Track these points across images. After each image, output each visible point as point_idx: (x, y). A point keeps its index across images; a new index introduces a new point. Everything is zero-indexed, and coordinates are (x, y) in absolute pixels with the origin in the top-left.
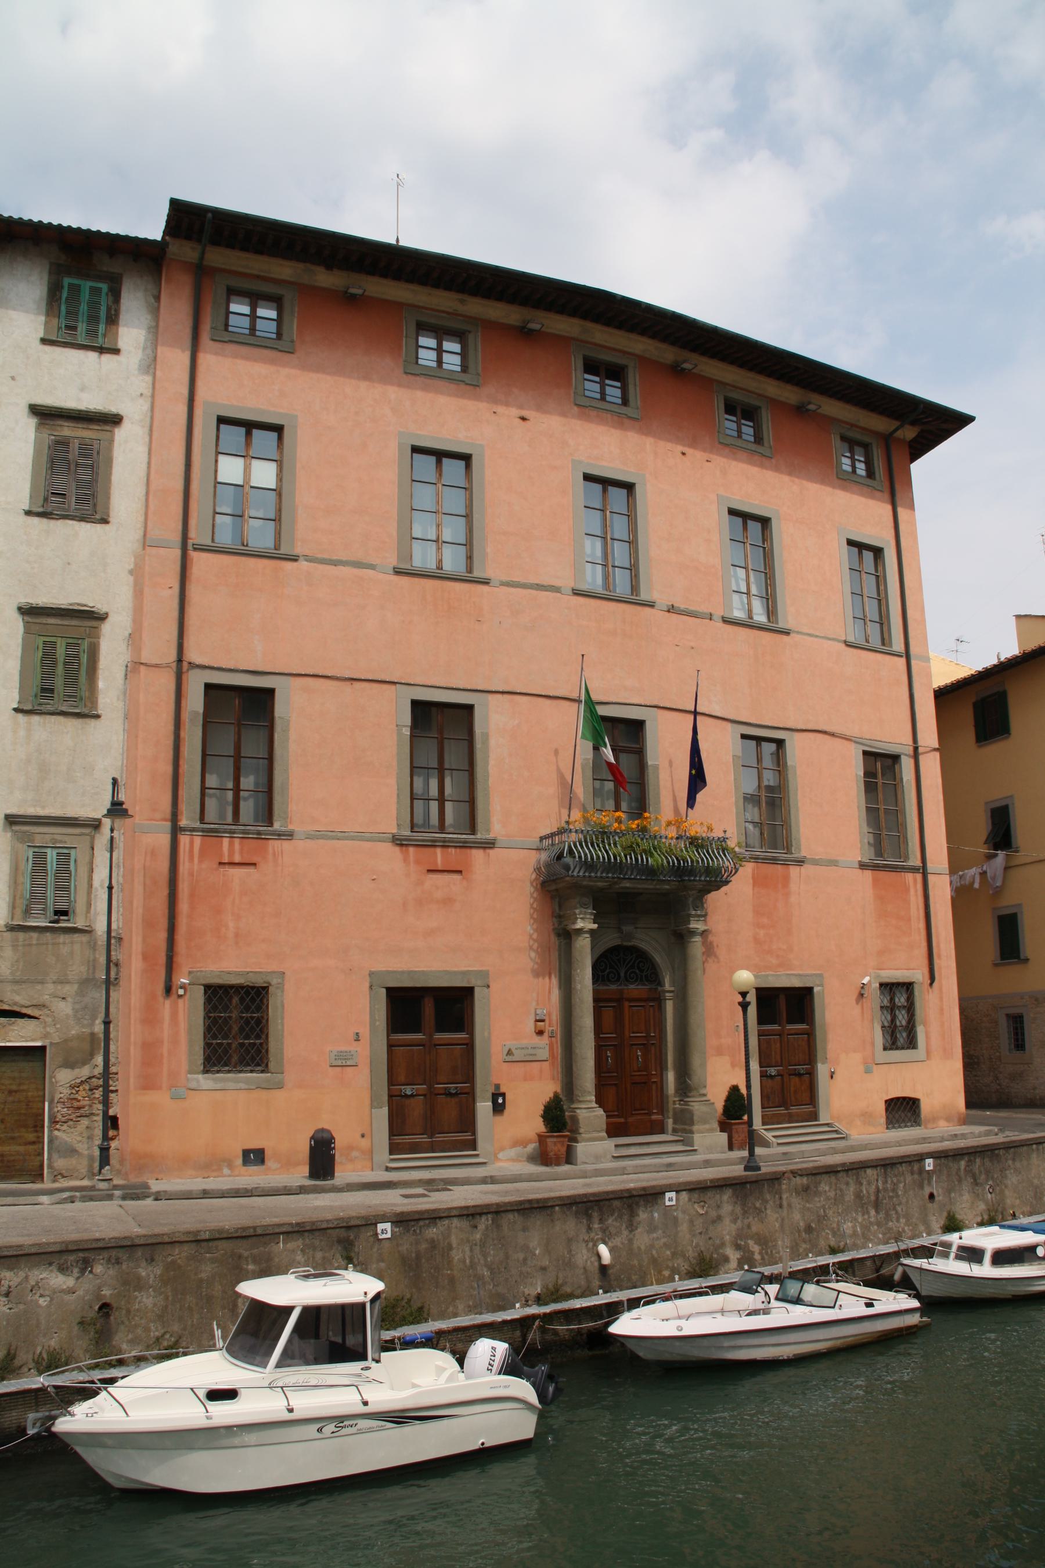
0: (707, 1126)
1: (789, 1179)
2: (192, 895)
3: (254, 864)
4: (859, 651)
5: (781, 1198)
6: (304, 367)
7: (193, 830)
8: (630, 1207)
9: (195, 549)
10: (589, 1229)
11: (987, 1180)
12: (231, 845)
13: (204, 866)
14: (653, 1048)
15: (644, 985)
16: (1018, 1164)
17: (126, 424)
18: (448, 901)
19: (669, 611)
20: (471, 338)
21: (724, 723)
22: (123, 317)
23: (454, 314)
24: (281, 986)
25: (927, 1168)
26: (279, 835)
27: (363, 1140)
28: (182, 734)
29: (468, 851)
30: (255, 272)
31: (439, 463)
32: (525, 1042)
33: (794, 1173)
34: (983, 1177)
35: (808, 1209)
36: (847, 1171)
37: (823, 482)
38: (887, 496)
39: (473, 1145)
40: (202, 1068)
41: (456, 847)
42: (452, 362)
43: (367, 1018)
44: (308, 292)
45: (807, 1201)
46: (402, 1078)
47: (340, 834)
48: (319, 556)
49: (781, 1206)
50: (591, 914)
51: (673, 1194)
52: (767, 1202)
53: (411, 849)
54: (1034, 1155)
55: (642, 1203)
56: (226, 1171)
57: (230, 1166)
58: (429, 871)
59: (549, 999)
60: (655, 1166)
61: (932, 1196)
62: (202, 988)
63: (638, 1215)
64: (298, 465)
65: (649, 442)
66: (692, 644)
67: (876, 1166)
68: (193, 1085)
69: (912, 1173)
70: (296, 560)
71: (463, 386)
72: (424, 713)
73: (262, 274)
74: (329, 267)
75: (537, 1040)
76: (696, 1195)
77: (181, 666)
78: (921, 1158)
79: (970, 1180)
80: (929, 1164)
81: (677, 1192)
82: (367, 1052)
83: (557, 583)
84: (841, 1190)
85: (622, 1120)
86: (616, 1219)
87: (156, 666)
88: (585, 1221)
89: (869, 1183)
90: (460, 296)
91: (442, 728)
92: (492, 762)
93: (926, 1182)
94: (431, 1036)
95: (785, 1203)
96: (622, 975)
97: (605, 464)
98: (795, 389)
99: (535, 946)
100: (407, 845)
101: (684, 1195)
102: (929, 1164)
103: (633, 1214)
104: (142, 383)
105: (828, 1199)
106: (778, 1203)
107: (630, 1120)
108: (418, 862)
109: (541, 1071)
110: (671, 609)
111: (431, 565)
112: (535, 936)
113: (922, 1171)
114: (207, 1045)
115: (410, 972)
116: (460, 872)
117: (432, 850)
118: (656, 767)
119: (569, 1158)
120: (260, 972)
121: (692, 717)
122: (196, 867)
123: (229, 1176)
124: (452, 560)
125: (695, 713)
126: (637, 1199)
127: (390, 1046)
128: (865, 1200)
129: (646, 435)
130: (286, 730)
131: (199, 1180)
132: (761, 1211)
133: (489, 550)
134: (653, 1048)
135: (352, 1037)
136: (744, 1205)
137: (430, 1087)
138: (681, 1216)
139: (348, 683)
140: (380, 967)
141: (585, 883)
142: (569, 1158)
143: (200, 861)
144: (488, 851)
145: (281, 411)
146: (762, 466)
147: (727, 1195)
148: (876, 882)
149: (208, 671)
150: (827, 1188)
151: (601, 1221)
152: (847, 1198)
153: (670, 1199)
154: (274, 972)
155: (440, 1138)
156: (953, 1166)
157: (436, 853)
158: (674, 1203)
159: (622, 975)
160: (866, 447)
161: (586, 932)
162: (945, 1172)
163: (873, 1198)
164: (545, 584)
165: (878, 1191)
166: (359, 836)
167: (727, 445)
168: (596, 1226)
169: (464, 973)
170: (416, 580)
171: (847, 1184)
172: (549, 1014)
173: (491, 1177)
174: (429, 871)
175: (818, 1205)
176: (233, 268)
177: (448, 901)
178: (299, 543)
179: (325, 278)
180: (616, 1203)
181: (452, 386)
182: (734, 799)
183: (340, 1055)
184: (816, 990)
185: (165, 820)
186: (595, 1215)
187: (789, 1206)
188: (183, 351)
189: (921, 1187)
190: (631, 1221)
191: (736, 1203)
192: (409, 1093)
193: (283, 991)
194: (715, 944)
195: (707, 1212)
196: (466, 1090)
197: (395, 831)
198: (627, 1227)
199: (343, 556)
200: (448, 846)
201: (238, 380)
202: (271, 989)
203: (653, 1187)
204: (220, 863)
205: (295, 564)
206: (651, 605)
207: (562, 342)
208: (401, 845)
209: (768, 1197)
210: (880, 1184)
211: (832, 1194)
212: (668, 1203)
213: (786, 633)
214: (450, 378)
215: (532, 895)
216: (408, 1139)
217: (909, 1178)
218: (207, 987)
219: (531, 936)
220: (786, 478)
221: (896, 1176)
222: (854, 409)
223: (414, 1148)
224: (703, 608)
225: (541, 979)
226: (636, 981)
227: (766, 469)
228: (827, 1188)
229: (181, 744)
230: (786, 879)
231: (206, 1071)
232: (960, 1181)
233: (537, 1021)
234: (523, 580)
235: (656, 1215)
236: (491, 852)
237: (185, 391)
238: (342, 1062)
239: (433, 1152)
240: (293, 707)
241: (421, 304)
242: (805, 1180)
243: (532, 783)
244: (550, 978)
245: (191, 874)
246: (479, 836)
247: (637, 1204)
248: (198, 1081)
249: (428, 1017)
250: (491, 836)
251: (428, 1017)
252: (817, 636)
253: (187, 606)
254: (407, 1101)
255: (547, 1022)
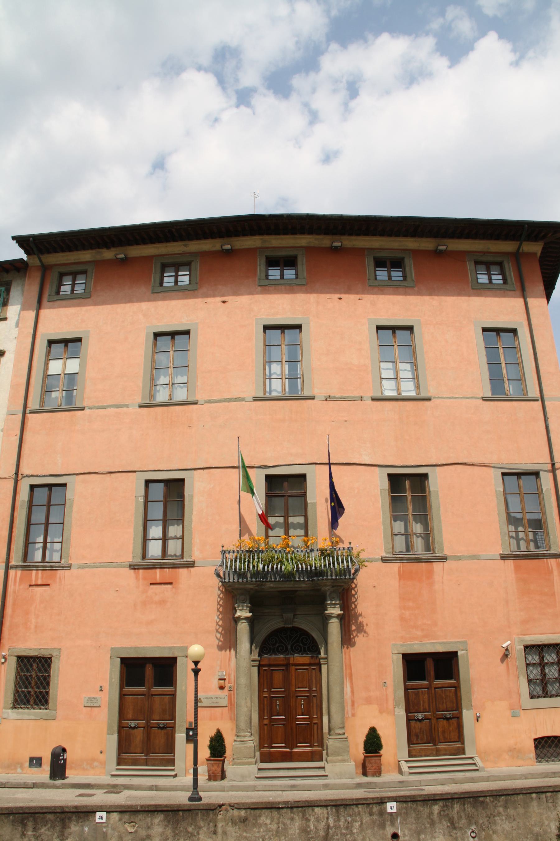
0: (340, 758)
1: (227, 810)
2: (14, 604)
3: (49, 585)
4: (496, 402)
5: (215, 826)
6: (95, 304)
7: (16, 567)
8: (63, 821)
9: (30, 413)
10: (23, 835)
11: (470, 824)
12: (37, 574)
13: (21, 587)
14: (315, 699)
15: (307, 654)
16: (511, 811)
17: (7, 355)
18: (162, 602)
19: (326, 400)
20: (193, 264)
21: (373, 468)
22: (11, 301)
23: (184, 254)
24: (59, 656)
25: (389, 811)
26: (63, 567)
27: (101, 755)
28: (15, 514)
29: (177, 570)
30: (73, 261)
31: (394, 333)
32: (211, 694)
33: (232, 806)
34: (464, 821)
35: (246, 837)
36: (292, 808)
37: (459, 294)
38: (519, 292)
39: (172, 762)
40: (12, 705)
41: (169, 568)
42: (184, 279)
43: (108, 676)
44: (99, 264)
45: (245, 831)
46: (130, 716)
47: (93, 564)
48: (96, 405)
49: (215, 833)
50: (247, 607)
51: (104, 814)
52: (200, 828)
53: (141, 571)
54: (535, 803)
55: (74, 818)
56: (19, 770)
57: (22, 767)
58: (151, 584)
59: (229, 665)
60: (281, 786)
61: (395, 836)
62: (16, 658)
63: (69, 828)
64: (88, 357)
65: (312, 297)
66: (346, 419)
67: (326, 806)
68: (5, 716)
69: (371, 814)
70: (83, 410)
71: (187, 292)
72: (396, 481)
73: (77, 261)
74: (108, 248)
75: (220, 693)
76: (126, 817)
77: (17, 477)
78: (382, 802)
79: (446, 823)
80: (392, 807)
81: (108, 812)
82: (107, 699)
83: (242, 395)
84: (284, 824)
85: (288, 750)
86: (48, 829)
87: (5, 478)
88: (20, 829)
89: (318, 820)
90: (184, 243)
91: (170, 495)
92: (195, 513)
93: (388, 823)
94: (149, 689)
95: (220, 830)
96: (289, 647)
97: (279, 317)
98: (429, 239)
99: (220, 630)
100: (138, 569)
101: (115, 816)
102: (392, 807)
103: (64, 826)
104: (15, 332)
105: (269, 830)
106: (213, 829)
107: (296, 750)
108: (144, 579)
109: (222, 714)
110: (328, 399)
111: (394, 393)
112: (220, 623)
113: (382, 813)
114: (16, 691)
115: (135, 648)
116: (171, 583)
117: (154, 570)
118: (314, 504)
119: (223, 776)
120: (47, 649)
121: (328, 466)
122: (17, 588)
123: (21, 773)
124: (408, 389)
125: (330, 464)
126: (70, 815)
127: (406, 689)
128: (312, 834)
129: (311, 293)
130: (71, 506)
131: (3, 774)
132: (192, 835)
133: (198, 384)
134: (315, 699)
135: (99, 689)
136: (175, 829)
137: (148, 722)
138: (110, 831)
139: (109, 475)
140: (118, 645)
141: (236, 586)
142: (223, 776)
143: (20, 585)
144: (190, 569)
145: (82, 330)
146: (406, 294)
147: (158, 819)
148: (402, 576)
149: (31, 478)
150: (268, 821)
151: (35, 829)
152: (290, 832)
153: (101, 818)
154: (55, 648)
155: (152, 756)
156: (425, 810)
157: (156, 573)
158: (104, 821)
159: (289, 647)
160: (500, 264)
161: (243, 619)
162: (414, 815)
163: (322, 833)
164: (235, 397)
165: (328, 827)
166: (109, 565)
167: (376, 286)
168: (30, 833)
169: (170, 648)
170: (152, 409)
171: (292, 819)
172: (229, 675)
173: (156, 786)
174: (151, 584)
175: (257, 835)
176: (62, 262)
177: (162, 602)
178: (86, 400)
179: (108, 254)
180: (50, 816)
181: (180, 294)
182: (381, 520)
183: (90, 700)
184: (459, 653)
185: (3, 562)
186: (30, 824)
187: (225, 833)
188: (33, 311)
189: (382, 826)
190: (62, 832)
191: (167, 826)
192: (133, 725)
193: (59, 660)
194: (364, 624)
195: (136, 831)
196: (172, 725)
197: (131, 560)
198: (58, 837)
199: (110, 403)
200: (164, 568)
201: (60, 320)
202: (53, 658)
203: (85, 806)
204: (30, 585)
205: (83, 412)
206: (312, 398)
207: (251, 252)
208: (135, 569)
209: (202, 824)
210: (331, 822)
211: (274, 827)
212: (98, 820)
213: (429, 399)
214: (183, 289)
215: (219, 596)
216: (131, 756)
217: (366, 819)
218: (19, 657)
219: (217, 623)
220: (427, 298)
221: (350, 815)
222: (483, 242)
223: (135, 762)
224: (357, 394)
225: (223, 651)
226: (300, 651)
227: (409, 295)
228: (268, 821)
229: (15, 520)
230: (430, 574)
231: (14, 707)
232: (433, 823)
233: (220, 679)
234: (219, 398)
235: (86, 829)
236: (192, 569)
237: (31, 331)
238: (92, 705)
239: (147, 766)
240: (437, 482)
241: (164, 253)
242: (243, 813)
243: (222, 521)
244: (230, 651)
245: (14, 592)
246: (185, 560)
247: (70, 819)
248: (8, 714)
249: (147, 678)
250: (192, 559)
251: (147, 678)
252: (456, 398)
253: (23, 444)
254: (133, 731)
255: (227, 681)
